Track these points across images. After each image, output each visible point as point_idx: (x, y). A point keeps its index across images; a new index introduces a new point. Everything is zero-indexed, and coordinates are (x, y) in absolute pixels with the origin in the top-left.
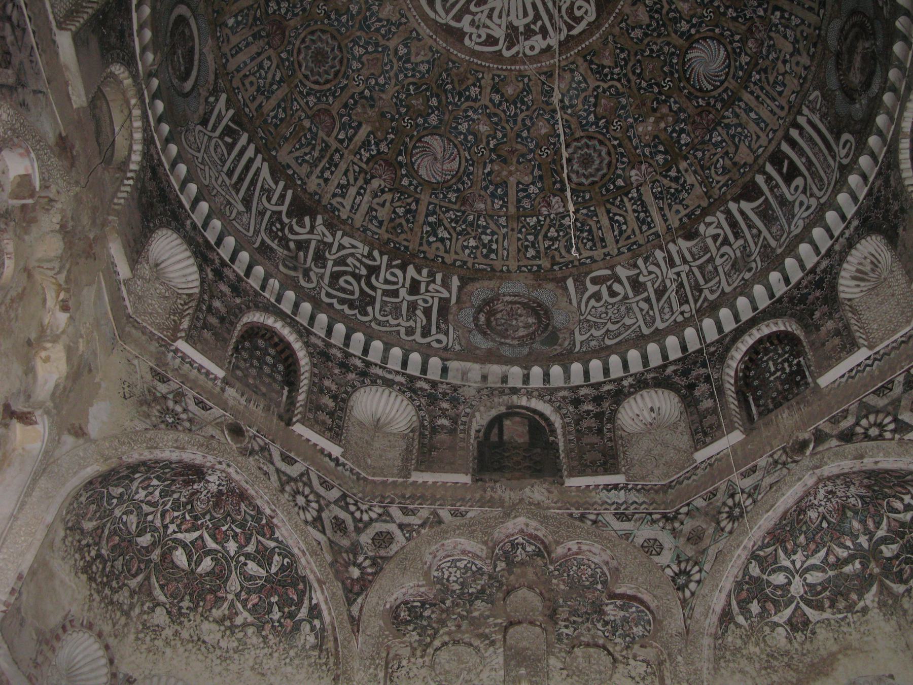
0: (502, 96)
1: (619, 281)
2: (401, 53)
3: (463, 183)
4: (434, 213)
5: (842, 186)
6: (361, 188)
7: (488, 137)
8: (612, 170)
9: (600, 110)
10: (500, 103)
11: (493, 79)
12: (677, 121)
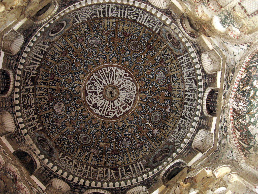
0: (82, 113)
1: (72, 163)
2: (75, 85)
3: (59, 117)
4: (49, 115)
5: (141, 176)
6: (44, 94)
7: (72, 116)
8: (89, 145)
9: (96, 134)
10: (80, 113)
11: (83, 108)
12: (110, 148)
